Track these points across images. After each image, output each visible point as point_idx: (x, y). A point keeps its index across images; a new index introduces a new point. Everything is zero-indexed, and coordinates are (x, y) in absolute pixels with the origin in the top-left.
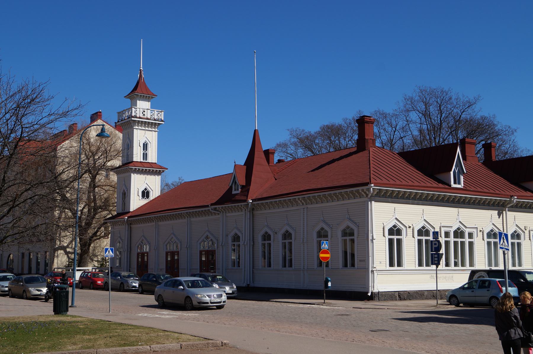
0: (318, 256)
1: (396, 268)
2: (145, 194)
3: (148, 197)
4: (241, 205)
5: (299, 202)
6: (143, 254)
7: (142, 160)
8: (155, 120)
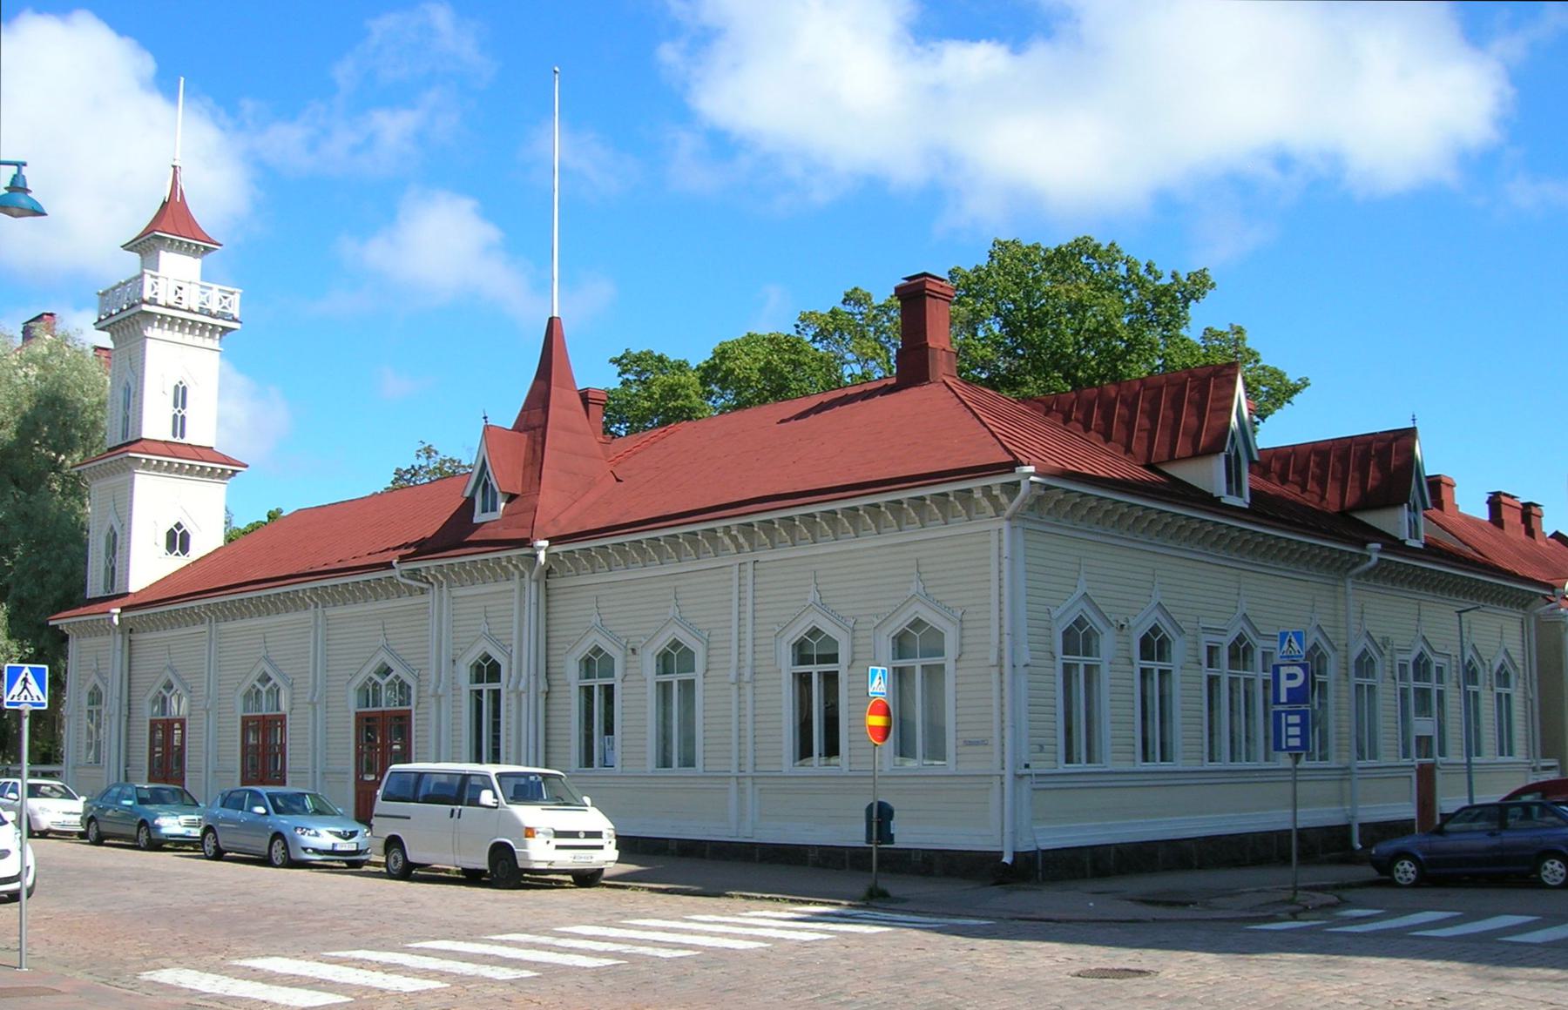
0: (57, 685)
1: (1082, 766)
2: (177, 540)
3: (185, 549)
4: (509, 559)
5: (727, 540)
6: (168, 726)
7: (170, 438)
8: (210, 315)
